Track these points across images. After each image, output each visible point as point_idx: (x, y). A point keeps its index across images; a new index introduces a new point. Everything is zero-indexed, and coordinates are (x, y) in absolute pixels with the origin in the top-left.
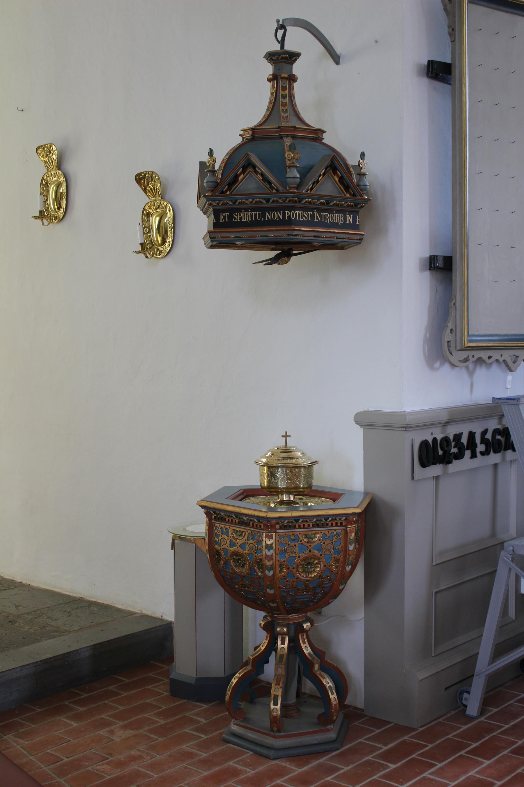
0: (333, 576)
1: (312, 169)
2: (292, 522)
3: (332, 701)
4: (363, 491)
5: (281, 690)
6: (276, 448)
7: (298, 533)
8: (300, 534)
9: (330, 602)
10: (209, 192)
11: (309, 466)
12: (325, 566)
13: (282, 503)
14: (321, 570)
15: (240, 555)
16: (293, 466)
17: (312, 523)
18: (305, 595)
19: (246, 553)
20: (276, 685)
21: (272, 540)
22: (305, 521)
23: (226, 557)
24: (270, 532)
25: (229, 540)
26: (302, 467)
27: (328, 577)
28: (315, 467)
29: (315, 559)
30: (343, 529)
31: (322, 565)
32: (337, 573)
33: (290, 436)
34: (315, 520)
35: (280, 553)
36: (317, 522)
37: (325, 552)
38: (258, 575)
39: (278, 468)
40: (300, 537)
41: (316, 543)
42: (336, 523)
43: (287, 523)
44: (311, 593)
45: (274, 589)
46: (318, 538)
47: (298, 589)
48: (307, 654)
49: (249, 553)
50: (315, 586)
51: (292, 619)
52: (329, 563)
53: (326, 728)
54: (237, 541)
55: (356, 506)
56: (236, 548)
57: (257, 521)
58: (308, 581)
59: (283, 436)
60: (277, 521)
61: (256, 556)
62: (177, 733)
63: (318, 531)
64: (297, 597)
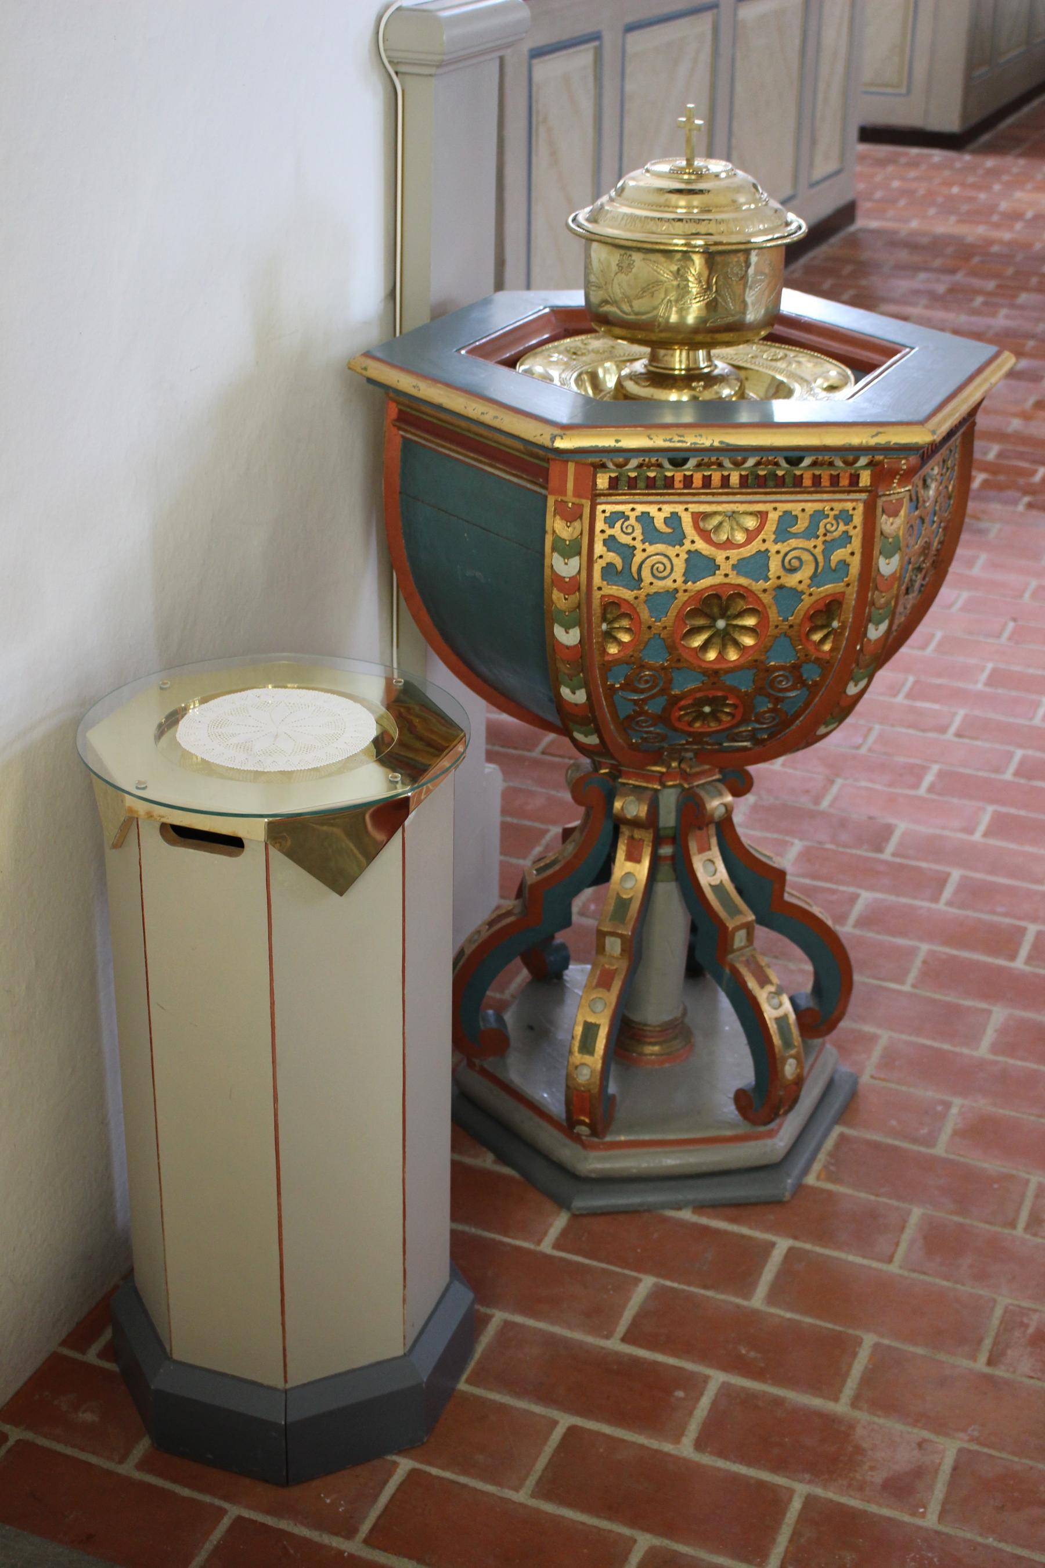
1: (316, 769)
10: (424, 1385)
34: (751, 462)
42: (835, 480)
55: (920, 417)
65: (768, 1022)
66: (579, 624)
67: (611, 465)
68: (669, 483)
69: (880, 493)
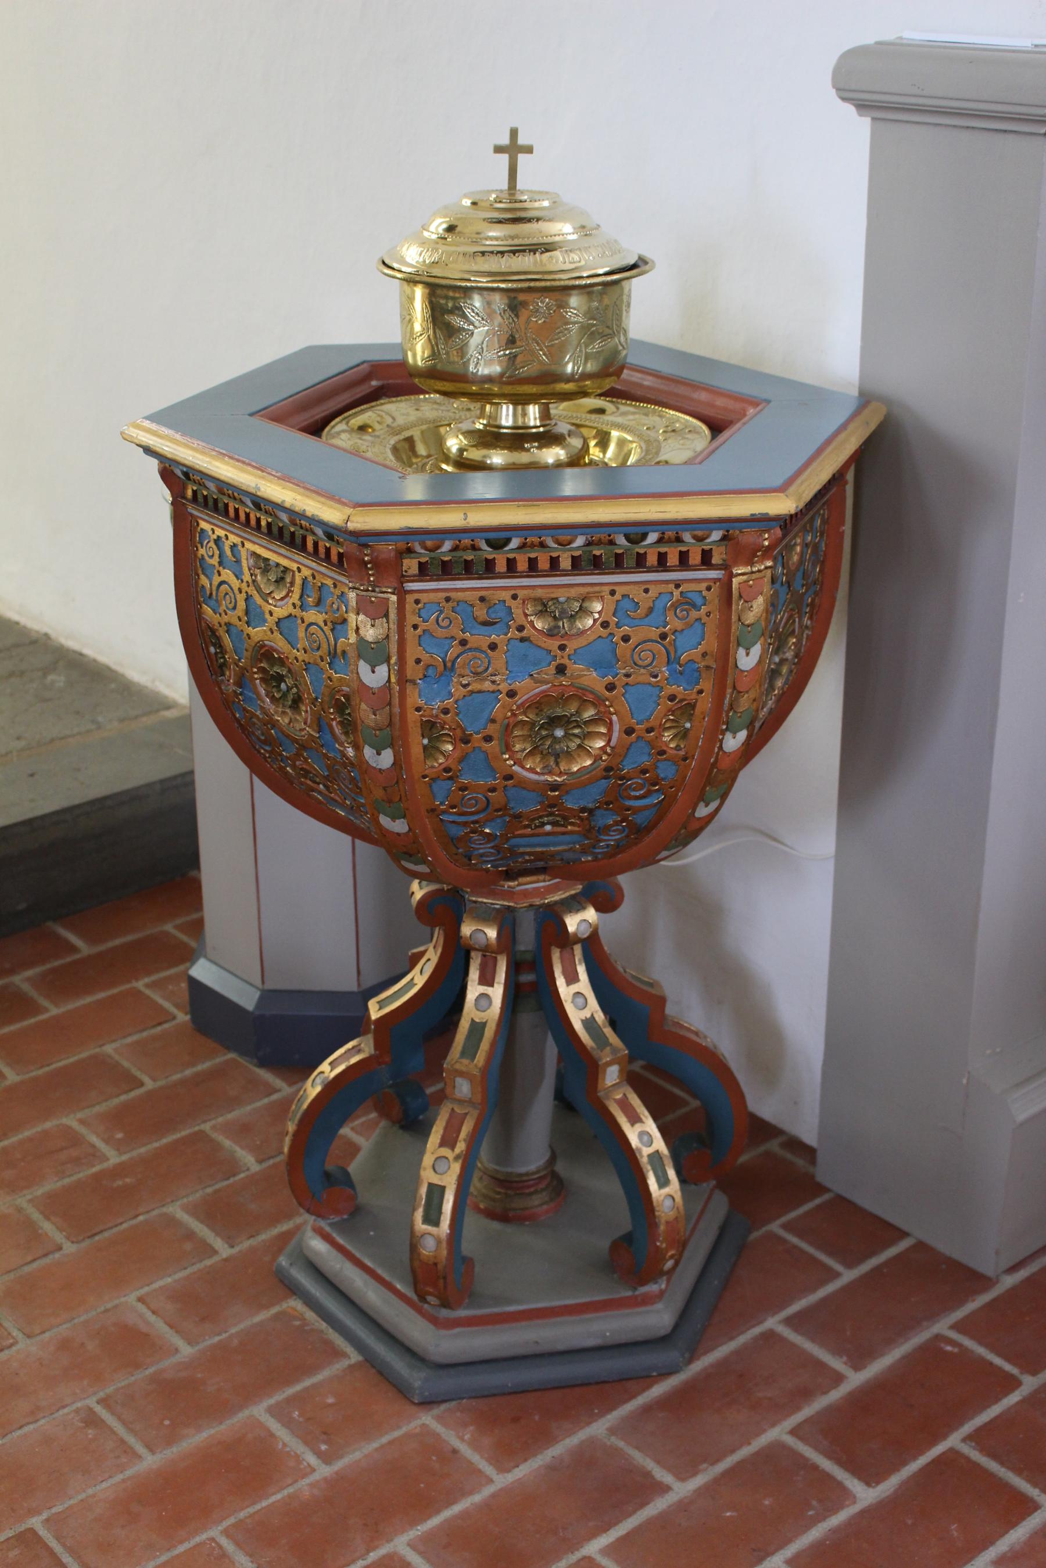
0: (666, 771)
2: (474, 548)
3: (657, 1213)
4: (855, 393)
5: (456, 1168)
8: (514, 597)
9: (659, 857)
12: (629, 731)
13: (492, 438)
14: (612, 748)
15: (281, 662)
16: (520, 285)
17: (569, 553)
18: (548, 834)
19: (300, 659)
20: (442, 1144)
21: (386, 625)
22: (533, 545)
23: (239, 660)
24: (373, 591)
25: (244, 595)
26: (574, 292)
27: (644, 771)
28: (637, 287)
29: (584, 703)
30: (715, 580)
31: (616, 727)
32: (685, 759)
33: (529, 150)
34: (580, 541)
35: (425, 676)
37: (627, 675)
38: (344, 755)
39: (467, 291)
40: (517, 612)
41: (591, 637)
42: (684, 557)
43: (451, 551)
44: (576, 829)
45: (404, 817)
46: (597, 616)
47: (518, 816)
48: (578, 1026)
49: (307, 660)
50: (590, 806)
51: (526, 894)
52: (648, 720)
53: (637, 1293)
54: (267, 602)
55: (778, 482)
56: (265, 631)
57: (325, 538)
58: (554, 787)
59: (499, 149)
60: (402, 545)
61: (330, 679)
62: (141, 1218)
63: (597, 589)
66: (392, 745)
69: (735, 572)
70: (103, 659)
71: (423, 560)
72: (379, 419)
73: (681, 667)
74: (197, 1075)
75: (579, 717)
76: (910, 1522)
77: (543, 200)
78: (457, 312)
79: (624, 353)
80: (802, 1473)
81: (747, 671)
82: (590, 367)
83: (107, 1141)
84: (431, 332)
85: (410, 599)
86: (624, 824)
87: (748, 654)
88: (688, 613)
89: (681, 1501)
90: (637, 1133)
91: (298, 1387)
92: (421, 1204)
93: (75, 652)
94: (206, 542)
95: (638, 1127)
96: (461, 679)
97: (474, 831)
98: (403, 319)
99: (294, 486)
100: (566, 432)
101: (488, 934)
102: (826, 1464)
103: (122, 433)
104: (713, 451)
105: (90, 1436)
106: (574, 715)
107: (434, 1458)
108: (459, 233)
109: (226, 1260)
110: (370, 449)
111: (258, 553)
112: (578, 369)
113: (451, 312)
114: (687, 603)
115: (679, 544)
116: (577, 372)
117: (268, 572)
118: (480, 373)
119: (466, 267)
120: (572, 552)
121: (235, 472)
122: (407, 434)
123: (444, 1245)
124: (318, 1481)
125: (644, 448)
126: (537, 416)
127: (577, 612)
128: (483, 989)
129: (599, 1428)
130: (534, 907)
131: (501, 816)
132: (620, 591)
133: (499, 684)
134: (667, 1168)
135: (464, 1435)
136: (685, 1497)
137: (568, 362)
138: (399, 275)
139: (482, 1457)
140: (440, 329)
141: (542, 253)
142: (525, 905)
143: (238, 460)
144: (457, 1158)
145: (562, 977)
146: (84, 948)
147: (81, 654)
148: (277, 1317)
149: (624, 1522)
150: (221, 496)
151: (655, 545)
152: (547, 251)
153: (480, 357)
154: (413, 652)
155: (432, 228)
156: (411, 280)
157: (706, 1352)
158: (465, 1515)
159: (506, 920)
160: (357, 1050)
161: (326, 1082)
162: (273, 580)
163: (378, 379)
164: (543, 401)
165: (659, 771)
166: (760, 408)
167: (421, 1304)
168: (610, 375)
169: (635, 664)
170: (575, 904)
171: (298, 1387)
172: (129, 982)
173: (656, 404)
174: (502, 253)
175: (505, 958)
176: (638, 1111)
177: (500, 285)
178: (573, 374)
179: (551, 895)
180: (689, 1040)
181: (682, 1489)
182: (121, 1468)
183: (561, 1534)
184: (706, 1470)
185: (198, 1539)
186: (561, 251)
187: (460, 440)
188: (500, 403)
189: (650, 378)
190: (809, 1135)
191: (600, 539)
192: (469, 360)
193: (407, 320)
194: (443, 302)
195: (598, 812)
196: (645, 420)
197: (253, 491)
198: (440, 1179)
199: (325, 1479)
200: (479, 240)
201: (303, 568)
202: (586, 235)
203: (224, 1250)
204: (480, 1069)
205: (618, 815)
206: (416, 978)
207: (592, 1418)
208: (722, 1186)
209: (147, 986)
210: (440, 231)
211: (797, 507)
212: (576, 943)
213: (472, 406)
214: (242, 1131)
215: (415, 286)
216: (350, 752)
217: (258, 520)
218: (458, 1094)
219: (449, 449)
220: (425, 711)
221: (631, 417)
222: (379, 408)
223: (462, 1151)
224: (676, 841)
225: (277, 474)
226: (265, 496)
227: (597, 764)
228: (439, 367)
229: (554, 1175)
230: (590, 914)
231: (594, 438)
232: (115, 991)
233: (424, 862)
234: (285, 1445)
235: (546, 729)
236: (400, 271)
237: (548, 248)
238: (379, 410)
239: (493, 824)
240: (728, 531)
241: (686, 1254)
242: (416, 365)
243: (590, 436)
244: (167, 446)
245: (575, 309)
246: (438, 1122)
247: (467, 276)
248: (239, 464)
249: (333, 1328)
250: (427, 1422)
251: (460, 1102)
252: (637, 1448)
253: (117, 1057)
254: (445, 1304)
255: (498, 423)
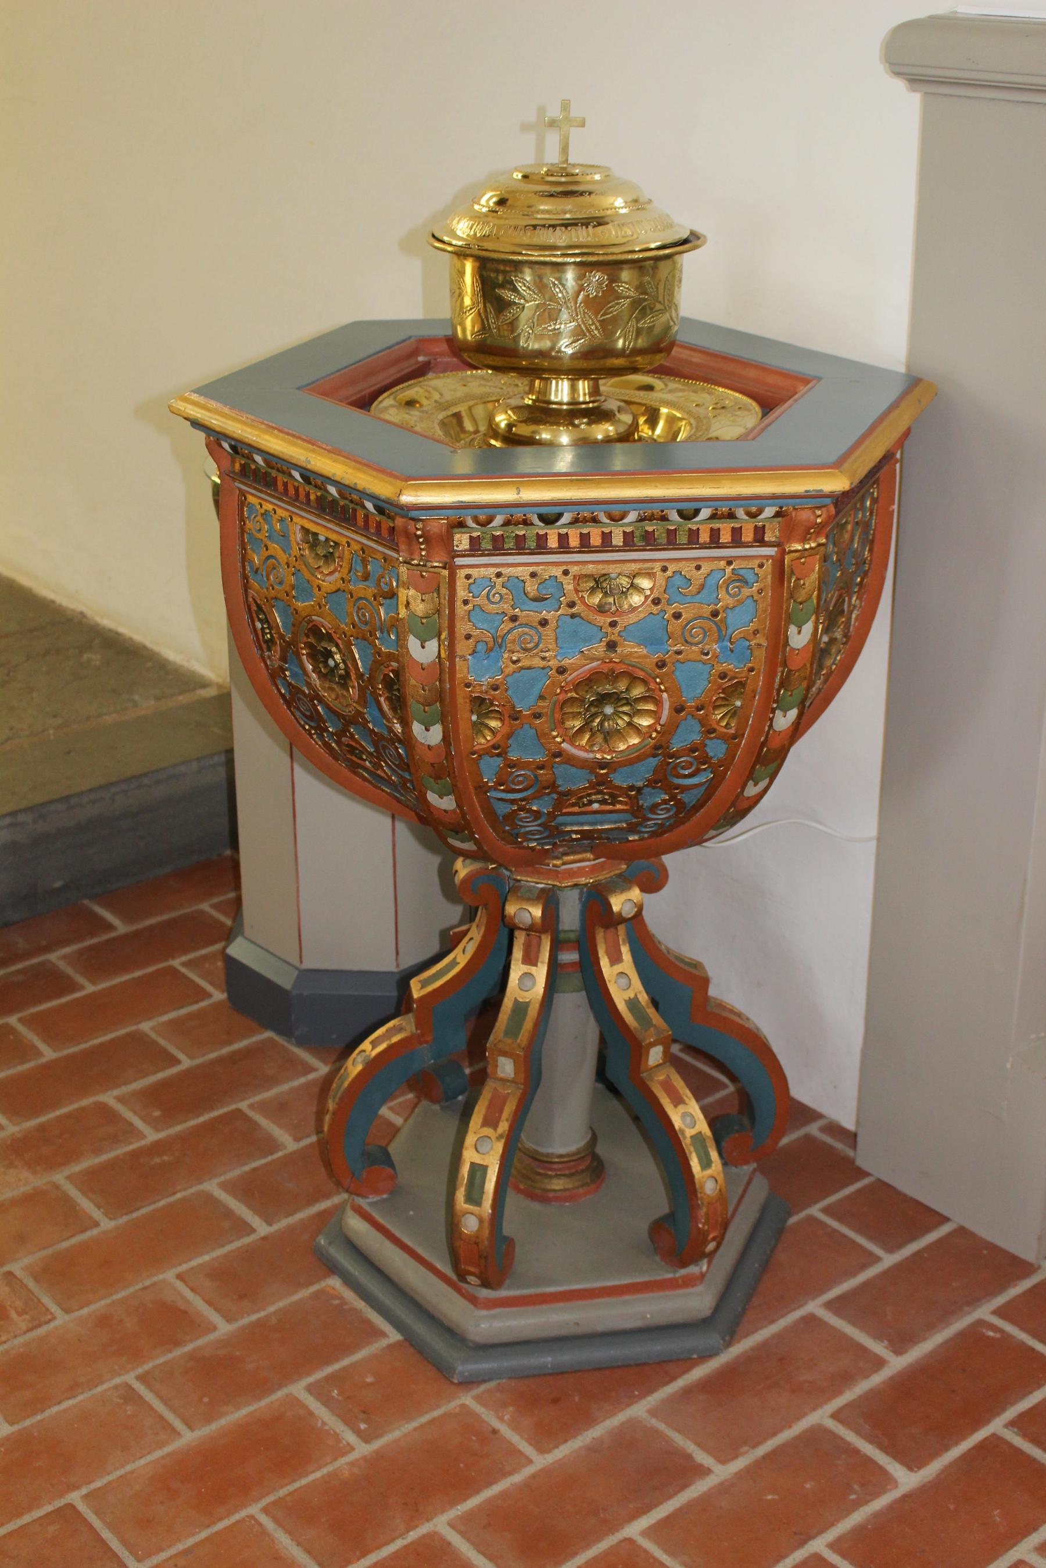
4: (902, 369)
5: (499, 1147)
6: (520, 176)
7: (557, 572)
9: (706, 837)
11: (657, 259)
12: (679, 709)
17: (621, 529)
26: (625, 266)
28: (689, 261)
29: (634, 679)
30: (768, 557)
31: (666, 705)
32: (734, 737)
34: (632, 517)
36: (642, 524)
38: (391, 730)
39: (517, 266)
42: (737, 533)
48: (621, 1006)
50: (640, 784)
51: (571, 874)
56: (313, 606)
58: (603, 765)
64: (561, 819)
65: (421, 995)
67: (470, 523)
68: (541, 546)
70: (138, 637)
71: (475, 534)
72: (427, 394)
73: (732, 644)
74: (234, 1053)
75: (628, 694)
76: (952, 1507)
77: (595, 174)
78: (508, 286)
79: (676, 328)
80: (844, 1456)
81: (798, 649)
82: (641, 343)
83: (143, 1119)
84: (481, 306)
85: (461, 573)
86: (672, 803)
87: (799, 632)
88: (739, 590)
89: (721, 1484)
90: (680, 1114)
91: (337, 1366)
92: (463, 1183)
93: (110, 630)
94: (253, 516)
95: (681, 1109)
96: (511, 655)
97: (522, 809)
98: (453, 294)
99: (345, 460)
100: (615, 409)
101: (533, 914)
102: (869, 1449)
103: (169, 407)
104: (763, 430)
105: (129, 1413)
106: (624, 692)
107: (474, 1438)
108: (510, 205)
109: (264, 1238)
110: (418, 424)
111: (306, 527)
112: (629, 345)
113: (502, 286)
114: (740, 579)
115: (732, 520)
116: (628, 348)
117: (316, 546)
118: (530, 347)
119: (517, 241)
120: (624, 528)
121: (284, 444)
122: (455, 410)
123: (486, 1225)
124: (357, 1460)
125: (694, 425)
126: (587, 391)
127: (628, 589)
128: (525, 968)
129: (640, 1410)
130: (579, 887)
131: (548, 794)
132: (672, 568)
133: (549, 661)
134: (709, 1149)
135: (503, 1416)
136: (726, 1480)
137: (619, 338)
138: (449, 249)
139: (522, 1437)
140: (491, 303)
141: (595, 226)
142: (569, 884)
143: (288, 434)
144: (499, 1137)
145: (606, 957)
146: (121, 927)
147: (117, 633)
148: (316, 1295)
149: (665, 1504)
150: (270, 470)
151: (708, 521)
152: (600, 224)
153: (530, 331)
154: (462, 628)
155: (483, 201)
156: (461, 254)
157: (747, 1335)
158: (504, 1495)
159: (549, 900)
160: (399, 1029)
161: (367, 1061)
162: (322, 555)
163: (425, 355)
164: (593, 376)
165: (708, 749)
166: (810, 385)
167: (461, 1284)
168: (659, 351)
169: (687, 642)
170: (623, 882)
171: (337, 1366)
172: (166, 960)
173: (705, 382)
174: (554, 226)
175: (549, 938)
176: (681, 1092)
177: (552, 258)
178: (624, 349)
179: (596, 875)
180: (732, 1022)
181: (722, 1472)
182: (161, 1445)
183: (602, 1515)
184: (746, 1453)
185: (237, 1517)
186: (614, 226)
187: (509, 415)
188: (548, 379)
189: (699, 355)
190: (848, 1123)
191: (653, 514)
192: (519, 335)
193: (458, 294)
194: (493, 275)
195: (646, 790)
196: (693, 397)
197: (304, 465)
198: (483, 1159)
199: (364, 1458)
200: (530, 213)
201: (352, 543)
202: (638, 209)
203: (262, 1229)
204: (523, 1049)
205: (666, 793)
206: (458, 957)
207: (632, 1400)
208: (761, 1169)
209: (184, 964)
210: (491, 203)
211: (851, 484)
212: (620, 923)
213: (518, 382)
214: (278, 1110)
215: (465, 259)
216: (398, 728)
217: (308, 495)
218: (500, 1074)
219: (497, 425)
220: (474, 687)
221: (680, 394)
222: (426, 383)
223: (504, 1131)
224: (724, 820)
225: (327, 448)
226: (315, 469)
227: (646, 742)
228: (488, 342)
229: (595, 1157)
230: (635, 894)
231: (643, 415)
232: (151, 969)
233: (471, 838)
234: (324, 1423)
235: (596, 706)
236: (450, 244)
237: (600, 222)
238: (427, 386)
239: (541, 802)
240: (781, 508)
241: (728, 1235)
242: (465, 340)
243: (639, 413)
244: (216, 419)
245: (626, 283)
246: (480, 1102)
247: (518, 250)
248: (289, 437)
249: (372, 1307)
250: (467, 1403)
251: (504, 1080)
252: (679, 1431)
253: (153, 1035)
254: (486, 1284)
255: (547, 399)
